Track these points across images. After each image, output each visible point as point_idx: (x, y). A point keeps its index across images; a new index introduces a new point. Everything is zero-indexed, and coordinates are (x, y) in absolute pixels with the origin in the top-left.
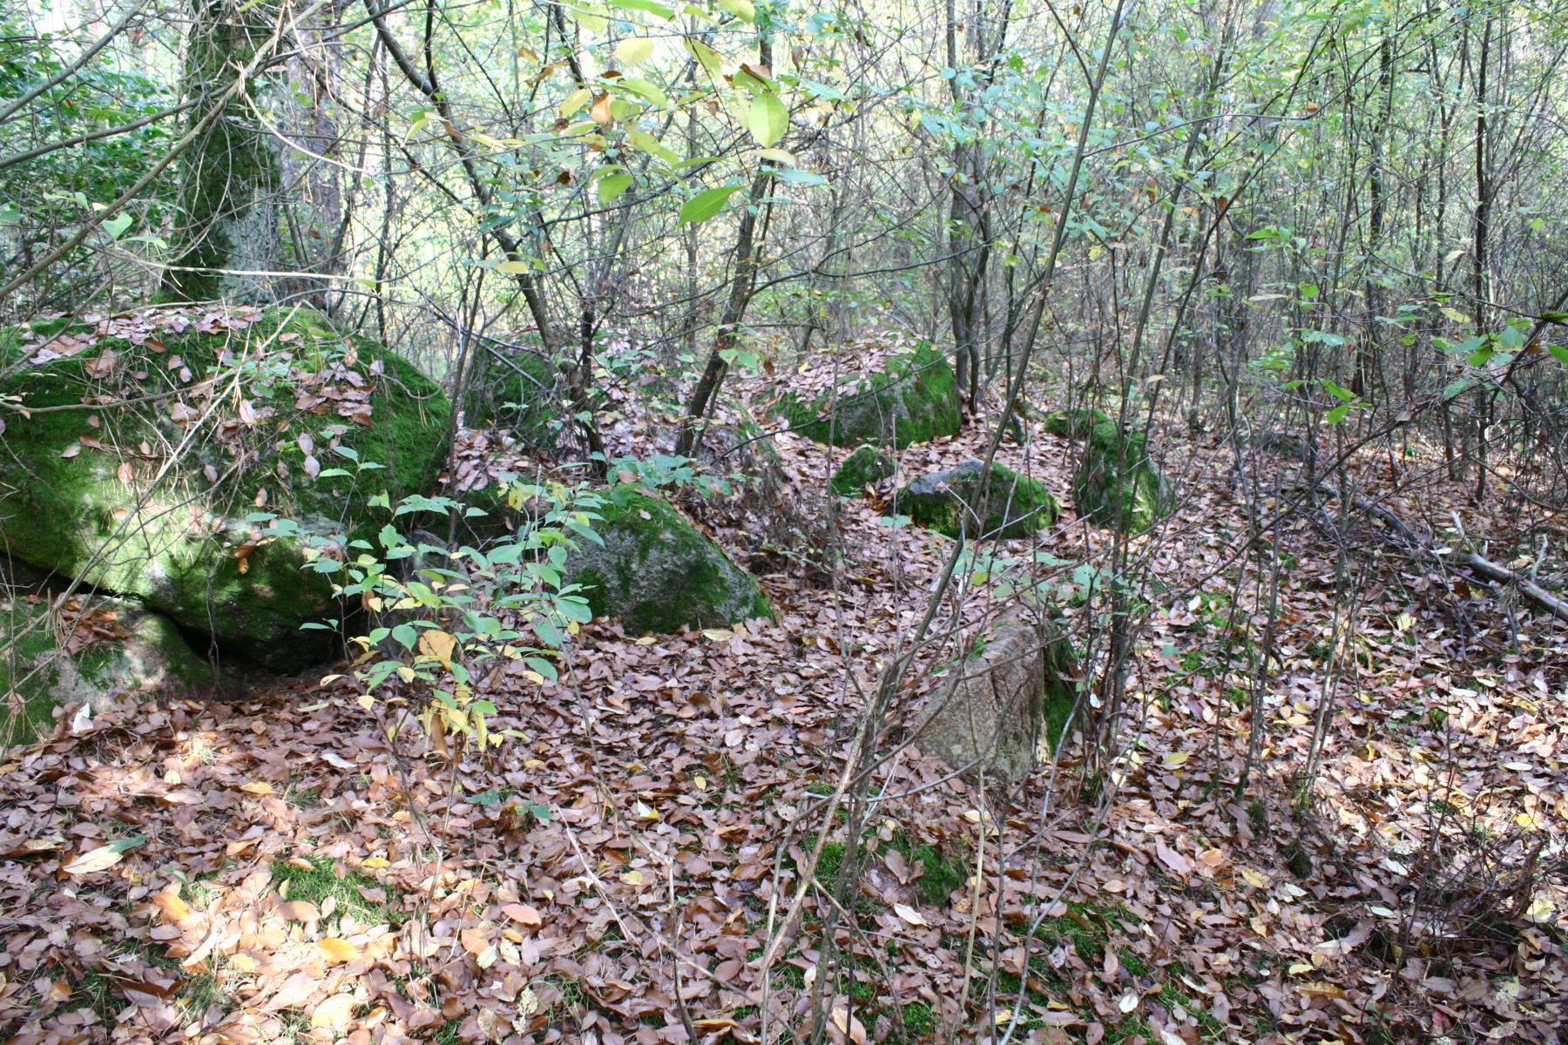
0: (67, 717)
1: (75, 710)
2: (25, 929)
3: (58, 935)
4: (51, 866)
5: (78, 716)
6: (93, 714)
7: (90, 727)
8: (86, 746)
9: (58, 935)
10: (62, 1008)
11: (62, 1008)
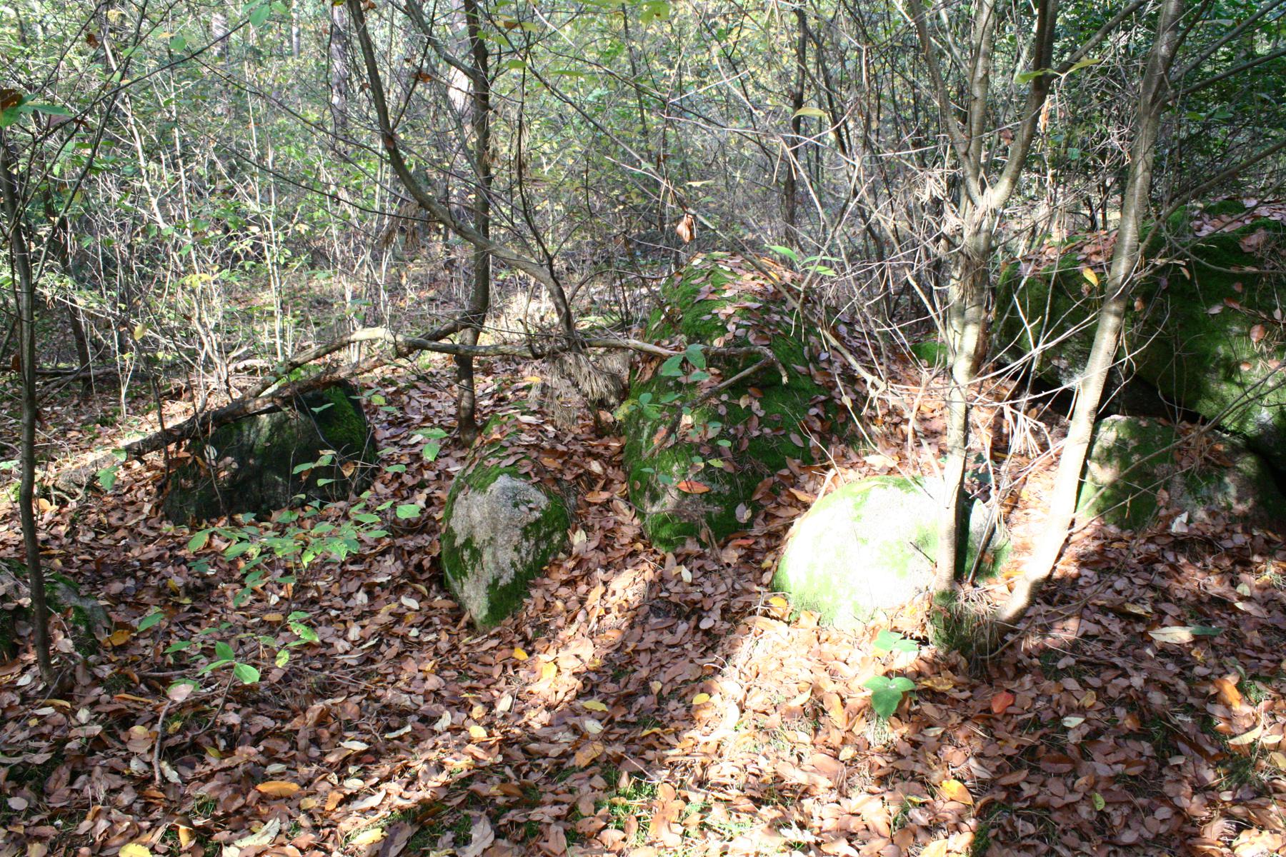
0: (1171, 518)
1: (1178, 514)
2: (1115, 666)
3: (1137, 681)
4: (1140, 628)
5: (1178, 520)
6: (1190, 520)
7: (1185, 530)
8: (1180, 544)
9: (1137, 681)
10: (1131, 735)
11: (1131, 735)
